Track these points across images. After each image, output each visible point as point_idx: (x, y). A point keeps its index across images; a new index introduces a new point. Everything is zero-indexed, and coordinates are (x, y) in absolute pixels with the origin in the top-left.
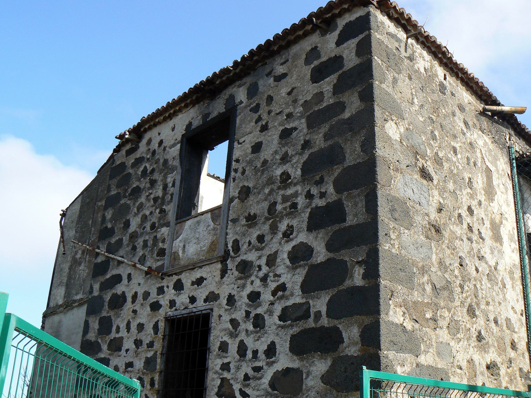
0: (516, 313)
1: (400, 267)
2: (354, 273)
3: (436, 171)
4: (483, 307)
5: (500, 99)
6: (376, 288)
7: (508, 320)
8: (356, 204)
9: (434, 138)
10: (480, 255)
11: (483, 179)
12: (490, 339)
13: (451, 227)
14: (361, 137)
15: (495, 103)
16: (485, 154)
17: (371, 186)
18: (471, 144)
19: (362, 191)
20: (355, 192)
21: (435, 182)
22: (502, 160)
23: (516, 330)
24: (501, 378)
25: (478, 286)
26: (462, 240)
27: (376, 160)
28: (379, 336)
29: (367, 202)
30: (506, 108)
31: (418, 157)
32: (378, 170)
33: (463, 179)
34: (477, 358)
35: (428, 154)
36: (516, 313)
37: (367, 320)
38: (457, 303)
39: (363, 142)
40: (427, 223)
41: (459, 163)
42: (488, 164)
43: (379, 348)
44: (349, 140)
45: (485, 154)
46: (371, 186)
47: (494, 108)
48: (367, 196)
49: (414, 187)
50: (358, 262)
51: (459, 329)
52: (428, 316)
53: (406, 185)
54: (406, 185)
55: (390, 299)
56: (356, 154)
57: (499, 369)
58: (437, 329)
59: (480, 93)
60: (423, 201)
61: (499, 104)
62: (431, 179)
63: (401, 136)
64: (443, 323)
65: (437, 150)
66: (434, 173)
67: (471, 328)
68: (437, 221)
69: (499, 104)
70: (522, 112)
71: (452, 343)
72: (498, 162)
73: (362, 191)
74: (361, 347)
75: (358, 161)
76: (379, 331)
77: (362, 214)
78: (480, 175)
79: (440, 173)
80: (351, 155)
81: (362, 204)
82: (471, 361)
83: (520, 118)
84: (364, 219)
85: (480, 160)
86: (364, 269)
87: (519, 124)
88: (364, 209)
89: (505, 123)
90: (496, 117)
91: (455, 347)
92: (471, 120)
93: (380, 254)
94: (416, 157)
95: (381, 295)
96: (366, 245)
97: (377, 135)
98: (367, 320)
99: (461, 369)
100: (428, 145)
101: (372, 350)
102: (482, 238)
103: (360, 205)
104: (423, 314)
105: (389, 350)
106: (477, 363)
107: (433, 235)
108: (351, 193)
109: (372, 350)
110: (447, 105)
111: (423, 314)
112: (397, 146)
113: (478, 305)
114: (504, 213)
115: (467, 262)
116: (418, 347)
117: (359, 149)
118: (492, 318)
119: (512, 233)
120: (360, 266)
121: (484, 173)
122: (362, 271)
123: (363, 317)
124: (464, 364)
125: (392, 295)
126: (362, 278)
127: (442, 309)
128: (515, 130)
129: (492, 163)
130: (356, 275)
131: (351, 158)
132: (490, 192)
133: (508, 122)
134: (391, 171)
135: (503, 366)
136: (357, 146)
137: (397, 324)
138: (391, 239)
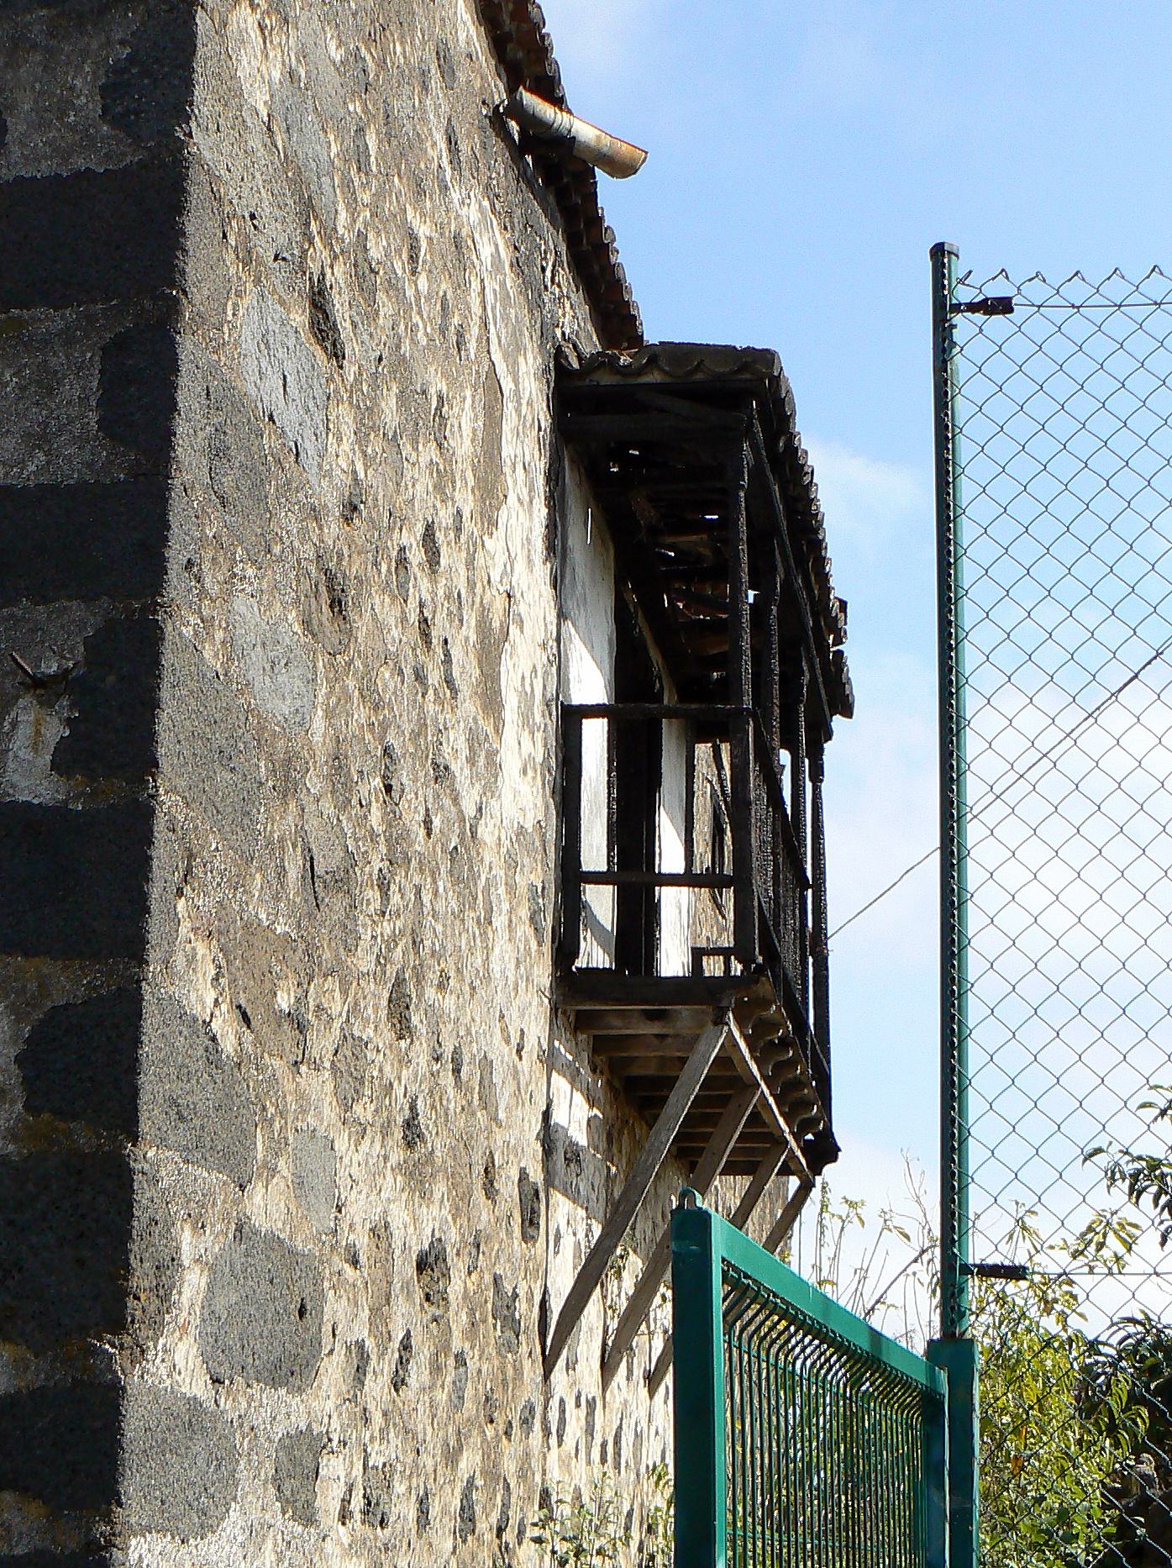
0: (508, 1042)
1: (220, 739)
2: (9, 736)
3: (357, 319)
4: (431, 993)
5: (569, 86)
6: (134, 826)
7: (486, 1064)
8: (47, 384)
9: (361, 159)
10: (439, 760)
11: (476, 418)
12: (437, 1143)
13: (377, 601)
14: (109, 43)
15: (549, 89)
16: (494, 308)
17: (147, 304)
18: (457, 242)
19: (90, 318)
20: (49, 320)
21: (351, 371)
22: (530, 355)
23: (502, 1115)
24: (451, 1313)
25: (426, 898)
26: (401, 673)
27: (185, 177)
28: (132, 1067)
29: (109, 384)
30: (585, 131)
31: (314, 227)
32: (190, 229)
33: (424, 392)
34: (399, 1217)
35: (341, 231)
36: (508, 1042)
37: (68, 984)
38: (364, 961)
39: (117, 70)
40: (312, 555)
41: (420, 313)
42: (497, 356)
43: (128, 1125)
44: (34, 47)
45: (494, 308)
46: (147, 304)
47: (546, 111)
48: (114, 351)
49: (289, 367)
50: (37, 684)
51: (361, 1080)
52: (284, 1001)
53: (267, 344)
54: (267, 344)
55: (180, 893)
56: (72, 128)
57: (446, 1275)
58: (303, 1068)
59: (508, 24)
60: (309, 446)
61: (559, 102)
62: (337, 354)
63: (272, 96)
64: (322, 1043)
65: (366, 225)
66: (348, 325)
67: (395, 1085)
68: (340, 556)
69: (559, 102)
70: (622, 168)
71: (342, 1144)
72: (521, 359)
73: (90, 318)
74: (18, 1120)
75: (80, 163)
76: (136, 1042)
77: (81, 441)
78: (468, 393)
79: (366, 337)
80: (41, 125)
81: (79, 390)
82: (380, 1232)
83: (608, 190)
84: (90, 465)
85: (475, 331)
86: (69, 722)
87: (595, 220)
88: (93, 417)
89: (551, 199)
90: (529, 159)
91: (346, 1160)
92: (468, 136)
93: (168, 658)
94: (307, 224)
95: (155, 863)
96: (88, 598)
97: (201, 52)
98: (68, 984)
99: (355, 1262)
100: (342, 186)
101: (84, 1137)
102: (449, 682)
103: (70, 389)
104: (268, 985)
105: (162, 1143)
106: (397, 1244)
107: (324, 619)
108: (20, 323)
109: (84, 1137)
110: (412, 29)
111: (268, 985)
112: (255, 142)
113: (419, 979)
114: (518, 596)
115: (405, 780)
116: (245, 1139)
117: (87, 102)
118: (448, 1050)
119: (528, 689)
120: (46, 703)
121: (480, 391)
122: (55, 731)
123: (47, 966)
124: (362, 1241)
125: (188, 872)
126: (54, 766)
127: (325, 976)
128: (572, 241)
129: (506, 356)
130: (20, 743)
131: (38, 141)
132: (490, 491)
133: (562, 196)
134: (230, 257)
135: (461, 1264)
136: (83, 87)
137: (195, 1020)
138: (203, 593)
